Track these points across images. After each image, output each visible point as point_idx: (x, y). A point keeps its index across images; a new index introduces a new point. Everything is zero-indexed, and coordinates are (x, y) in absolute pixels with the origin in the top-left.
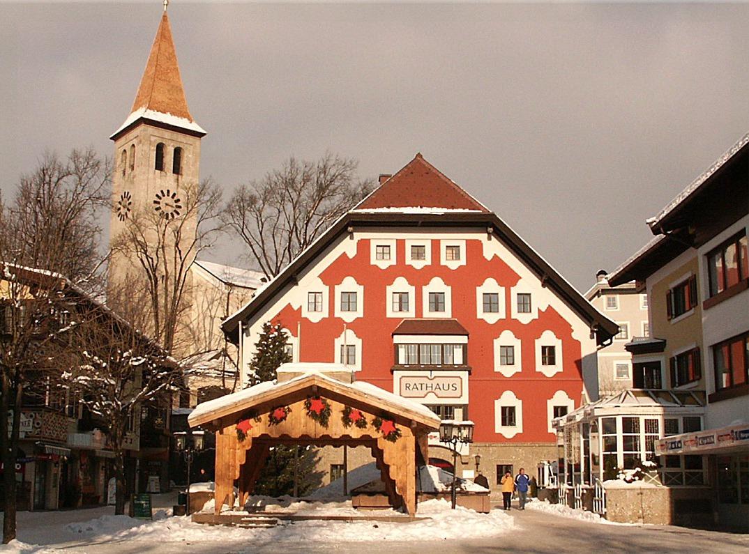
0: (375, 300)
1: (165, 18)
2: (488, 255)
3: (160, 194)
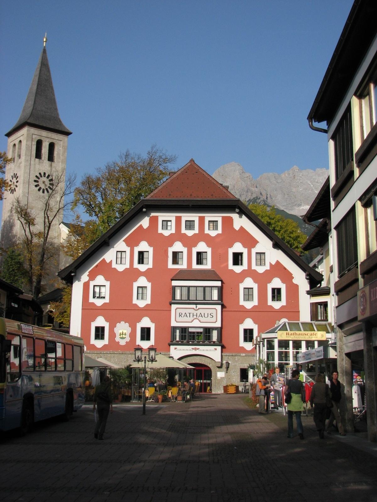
0: (160, 257)
1: (44, 51)
2: (237, 227)
3: (39, 176)
